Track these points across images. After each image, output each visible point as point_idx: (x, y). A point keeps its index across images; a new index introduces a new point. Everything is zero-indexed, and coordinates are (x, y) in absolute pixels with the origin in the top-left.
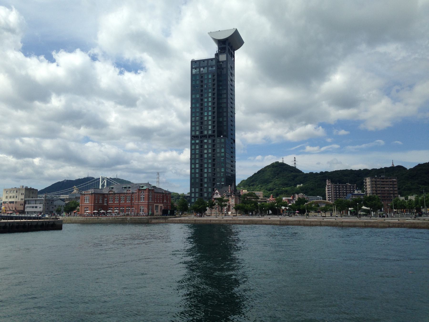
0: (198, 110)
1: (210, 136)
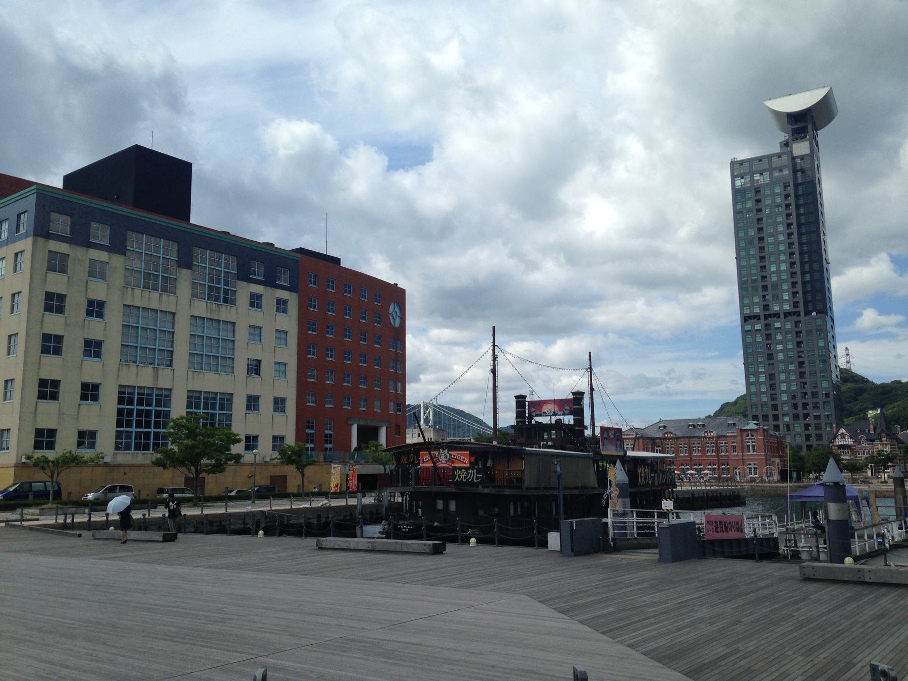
0: (753, 262)
1: (787, 314)
